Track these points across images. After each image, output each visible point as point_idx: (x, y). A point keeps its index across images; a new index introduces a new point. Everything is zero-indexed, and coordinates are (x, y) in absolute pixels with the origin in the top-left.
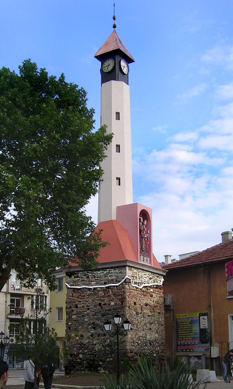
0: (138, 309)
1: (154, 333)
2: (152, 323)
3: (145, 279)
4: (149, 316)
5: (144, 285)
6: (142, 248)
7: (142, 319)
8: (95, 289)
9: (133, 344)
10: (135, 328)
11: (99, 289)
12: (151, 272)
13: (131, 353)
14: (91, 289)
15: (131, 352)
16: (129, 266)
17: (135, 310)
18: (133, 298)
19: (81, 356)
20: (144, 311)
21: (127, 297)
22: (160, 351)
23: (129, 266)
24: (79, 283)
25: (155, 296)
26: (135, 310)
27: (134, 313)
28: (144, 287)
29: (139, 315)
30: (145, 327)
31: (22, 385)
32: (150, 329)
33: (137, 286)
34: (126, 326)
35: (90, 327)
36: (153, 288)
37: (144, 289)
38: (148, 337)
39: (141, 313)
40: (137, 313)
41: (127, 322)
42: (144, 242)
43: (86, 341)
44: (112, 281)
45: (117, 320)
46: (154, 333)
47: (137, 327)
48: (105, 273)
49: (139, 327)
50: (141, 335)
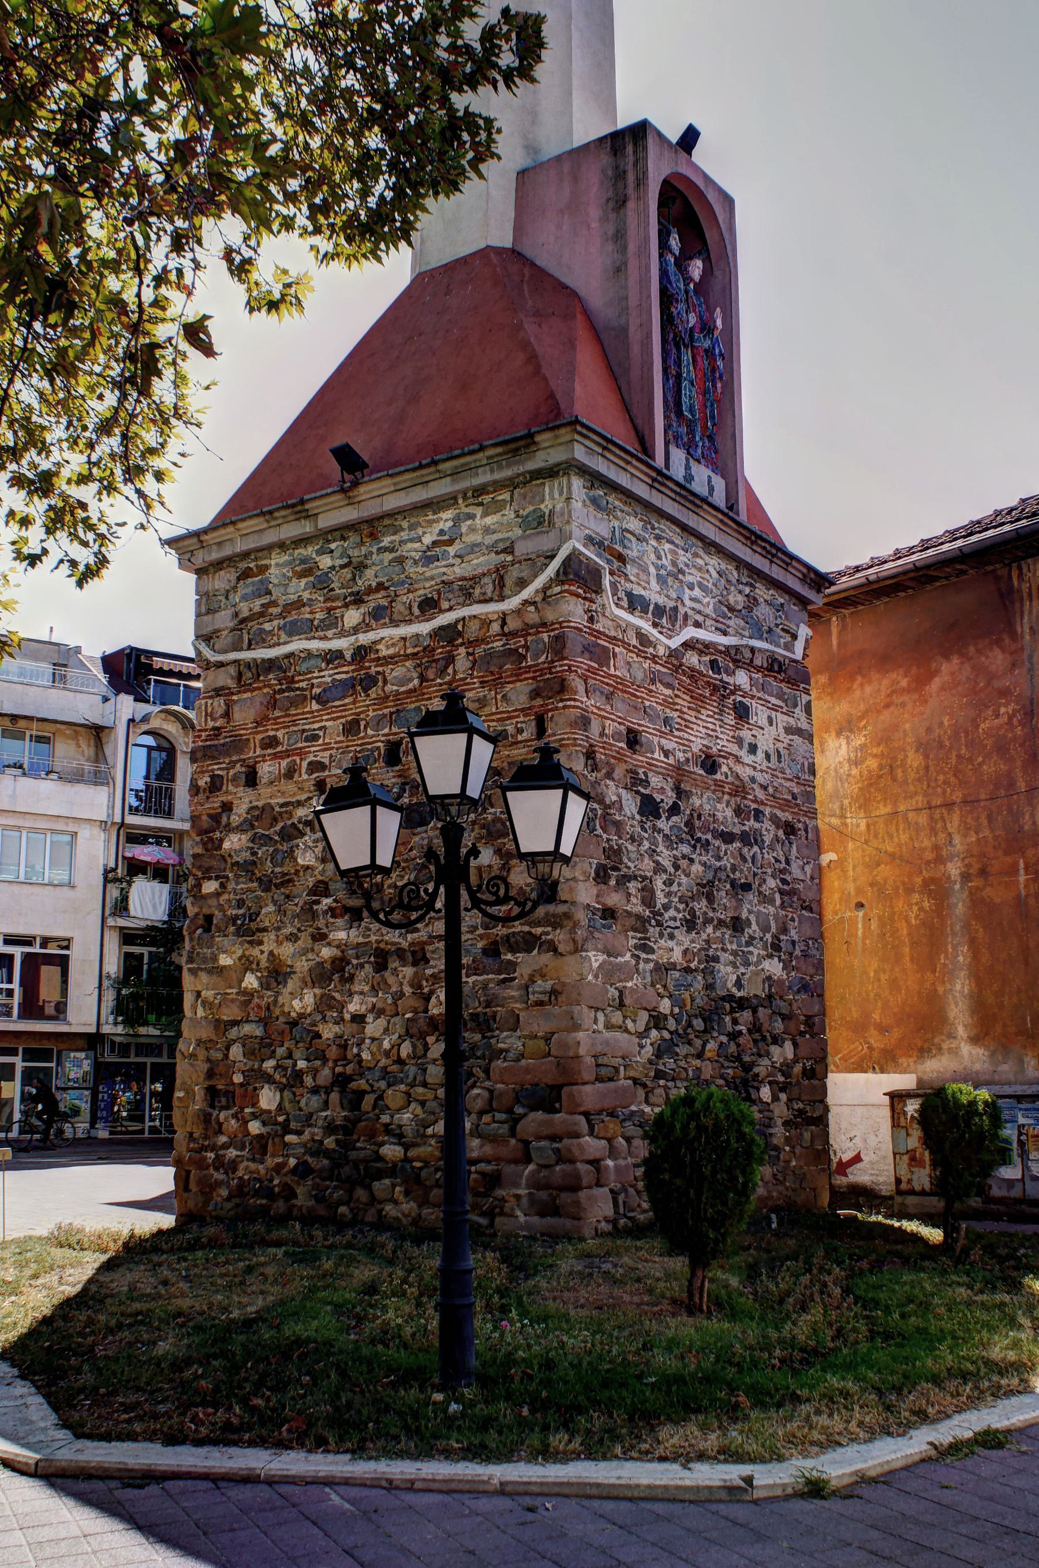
0: (655, 780)
1: (756, 951)
2: (747, 887)
3: (697, 592)
4: (728, 838)
5: (690, 633)
6: (678, 403)
7: (685, 849)
8: (361, 653)
9: (617, 1017)
10: (636, 906)
11: (384, 651)
12: (740, 563)
13: (599, 1079)
14: (339, 654)
15: (605, 1075)
16: (595, 479)
17: (635, 781)
18: (620, 707)
19: (268, 1099)
20: (696, 802)
21: (579, 685)
22: (798, 1068)
23: (595, 479)
24: (267, 627)
25: (763, 721)
26: (635, 781)
27: (630, 805)
28: (687, 645)
29: (662, 824)
30: (701, 906)
31: (839, 1071)
32: (736, 920)
33: (646, 626)
34: (538, 819)
35: (327, 901)
36: (749, 666)
37: (692, 659)
38: (727, 974)
39: (674, 810)
40: (649, 807)
41: (543, 772)
42: (688, 371)
43: (301, 1001)
44: (467, 590)
45: (444, 763)
46: (756, 951)
47: (649, 900)
48: (427, 540)
49: (661, 899)
50: (677, 956)
